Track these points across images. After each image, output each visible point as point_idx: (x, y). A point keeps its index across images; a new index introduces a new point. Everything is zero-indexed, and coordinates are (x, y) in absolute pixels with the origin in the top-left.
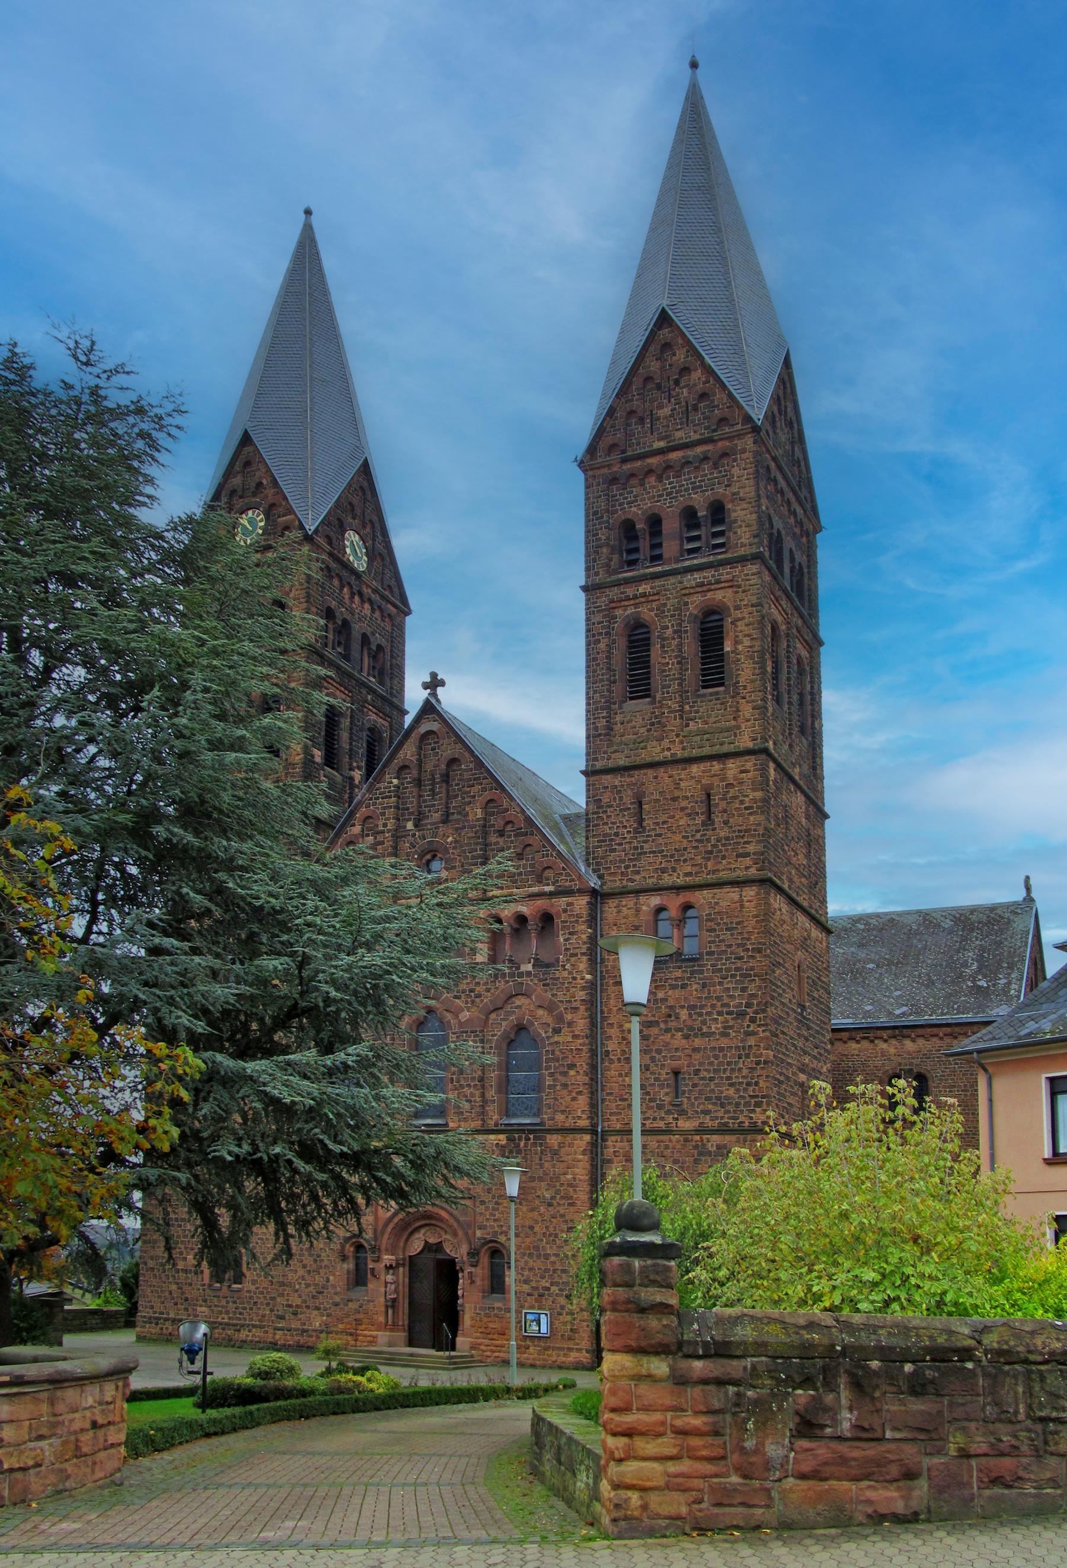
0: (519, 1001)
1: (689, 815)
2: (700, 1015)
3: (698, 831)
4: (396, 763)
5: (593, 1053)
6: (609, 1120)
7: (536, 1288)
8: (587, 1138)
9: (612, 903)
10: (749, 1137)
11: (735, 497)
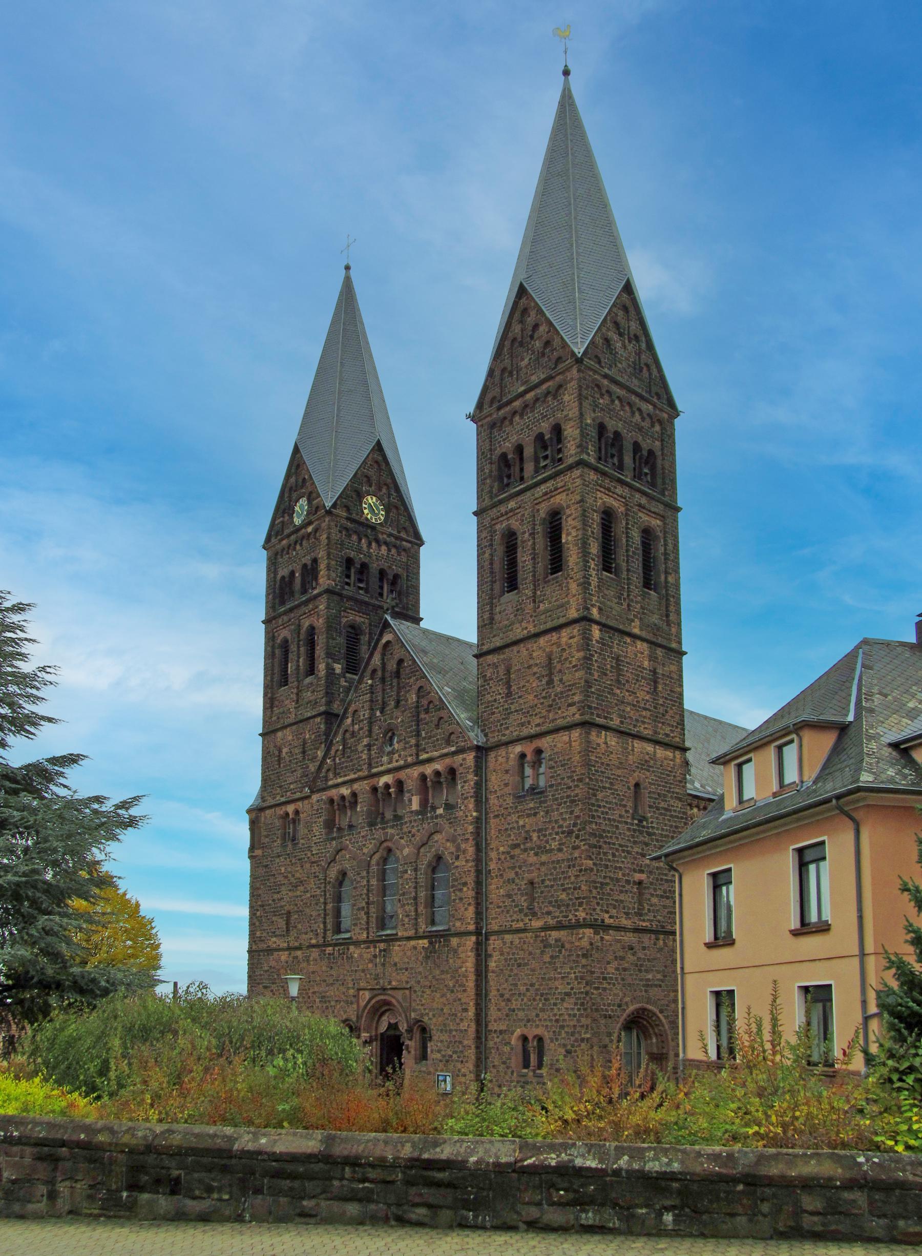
0: (437, 837)
1: (538, 678)
2: (545, 836)
3: (543, 690)
4: (370, 668)
5: (478, 872)
6: (491, 924)
8: (474, 938)
9: (492, 755)
10: (575, 931)
11: (567, 419)
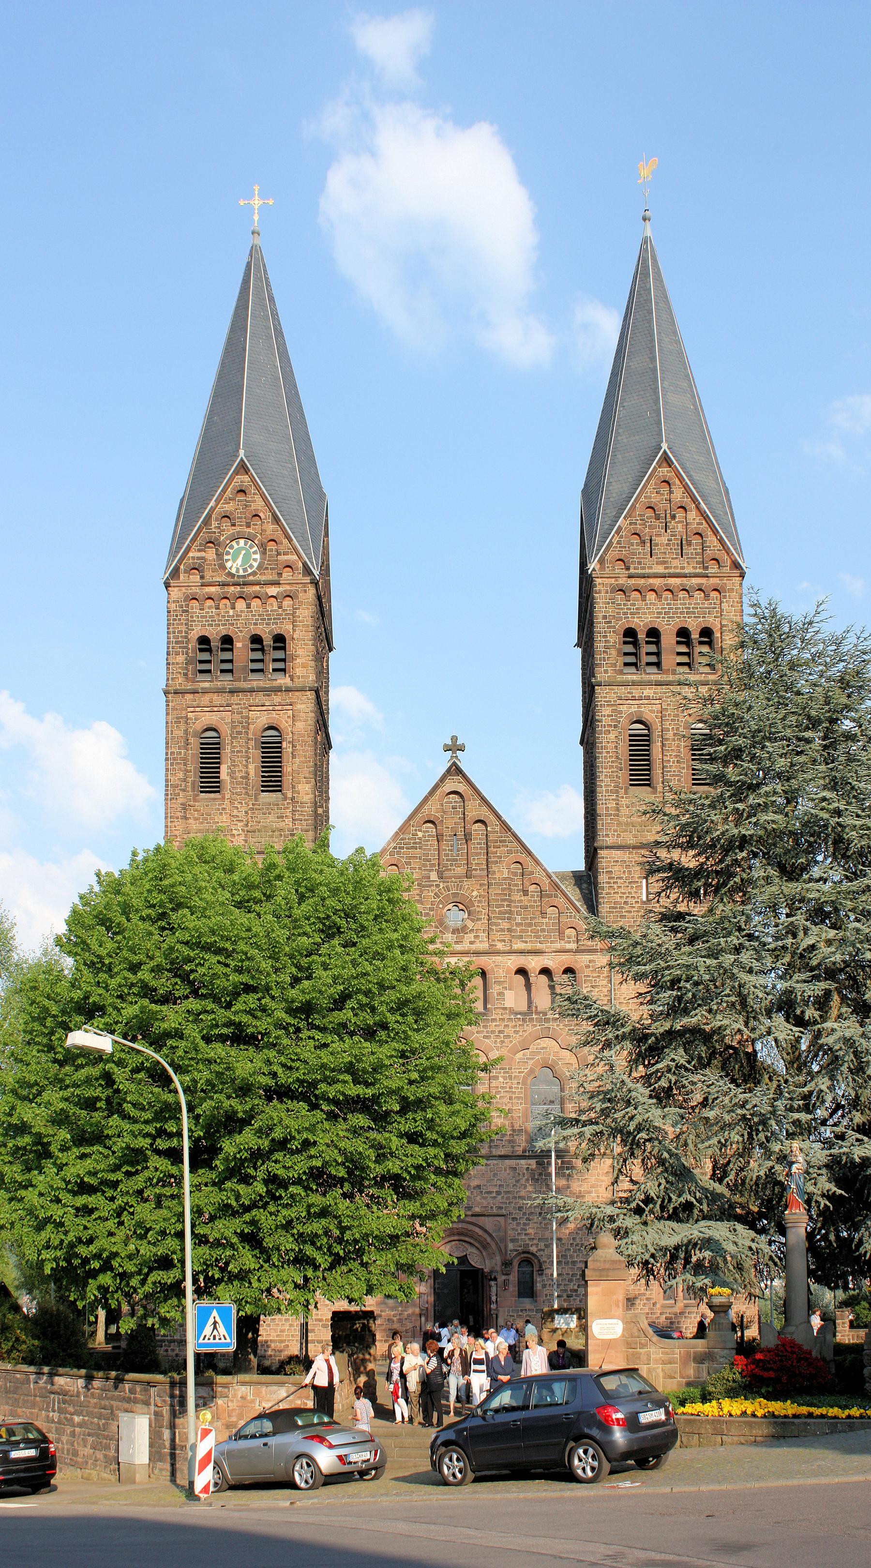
7: (566, 1291)
